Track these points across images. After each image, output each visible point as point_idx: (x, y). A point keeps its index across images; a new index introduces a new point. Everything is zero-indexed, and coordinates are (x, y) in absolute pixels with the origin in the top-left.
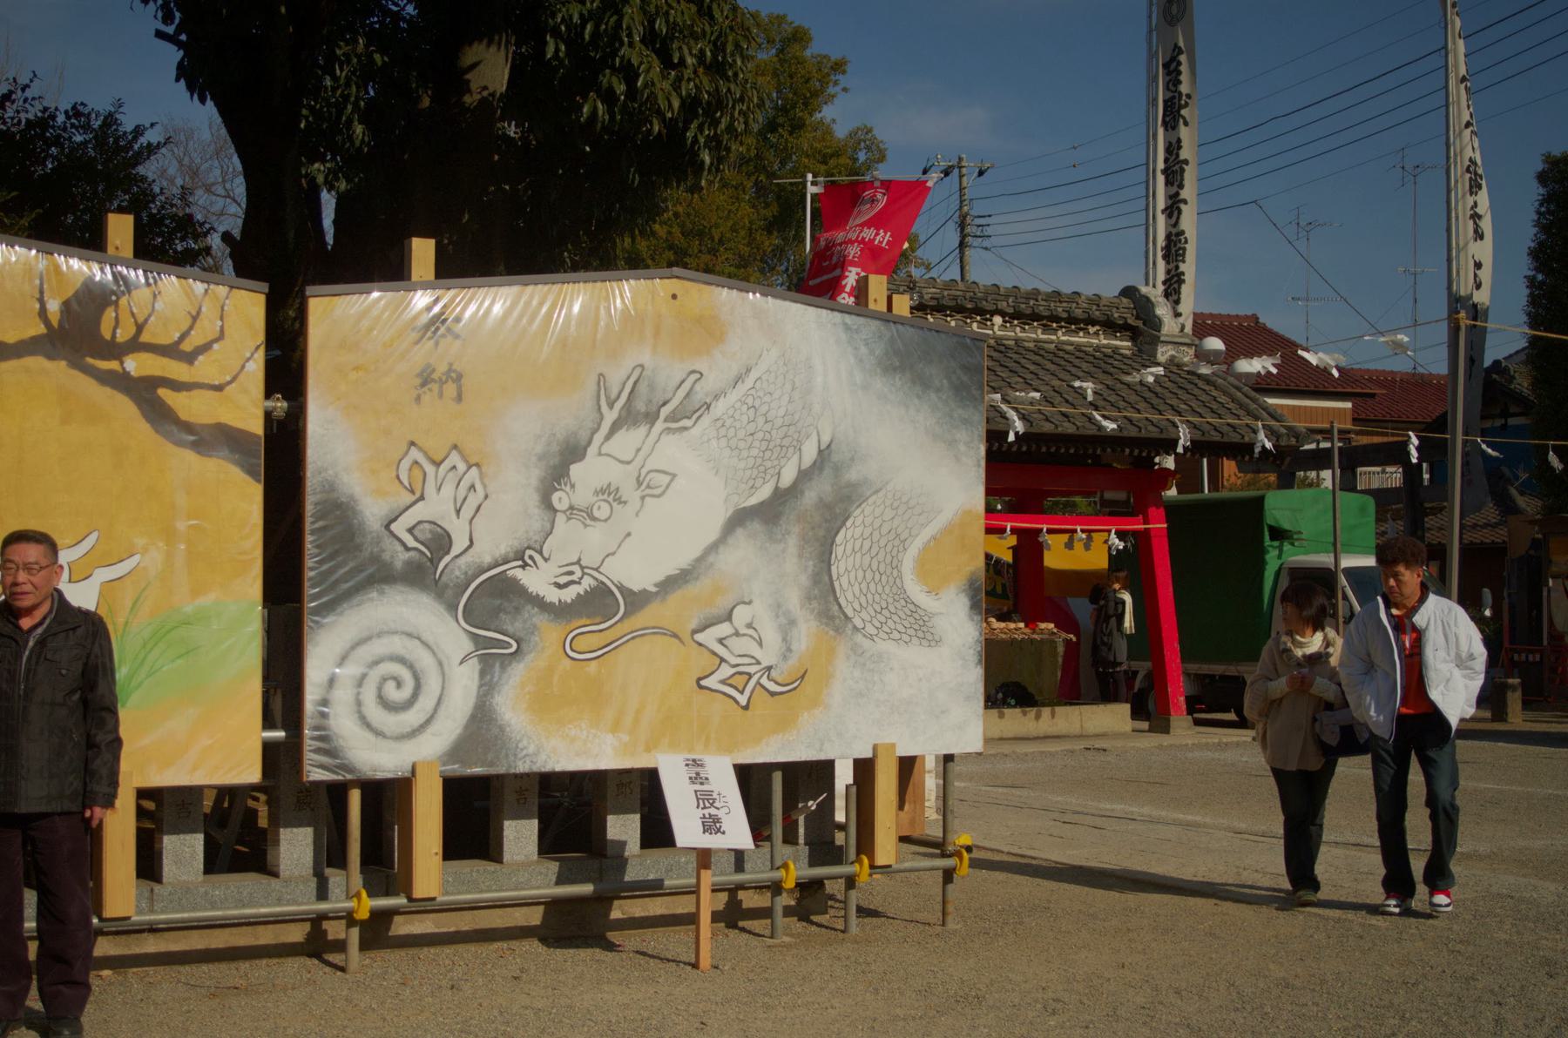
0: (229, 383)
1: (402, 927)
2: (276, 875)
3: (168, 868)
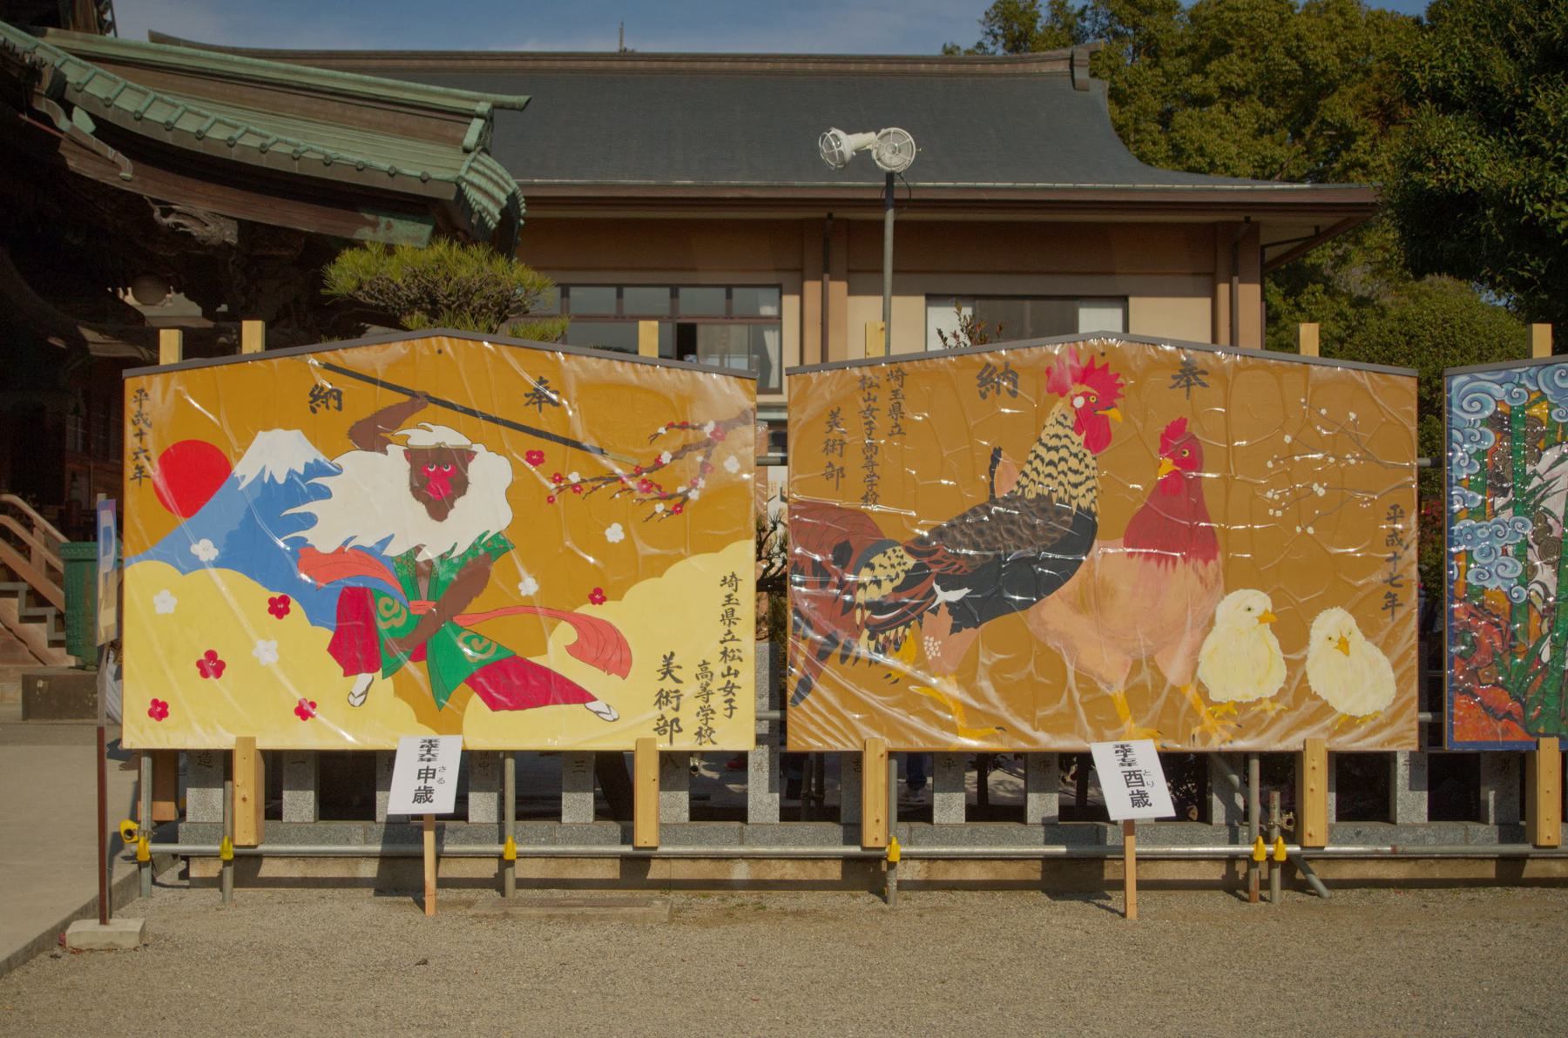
1: (1532, 869)
2: (1394, 823)
3: (289, 813)
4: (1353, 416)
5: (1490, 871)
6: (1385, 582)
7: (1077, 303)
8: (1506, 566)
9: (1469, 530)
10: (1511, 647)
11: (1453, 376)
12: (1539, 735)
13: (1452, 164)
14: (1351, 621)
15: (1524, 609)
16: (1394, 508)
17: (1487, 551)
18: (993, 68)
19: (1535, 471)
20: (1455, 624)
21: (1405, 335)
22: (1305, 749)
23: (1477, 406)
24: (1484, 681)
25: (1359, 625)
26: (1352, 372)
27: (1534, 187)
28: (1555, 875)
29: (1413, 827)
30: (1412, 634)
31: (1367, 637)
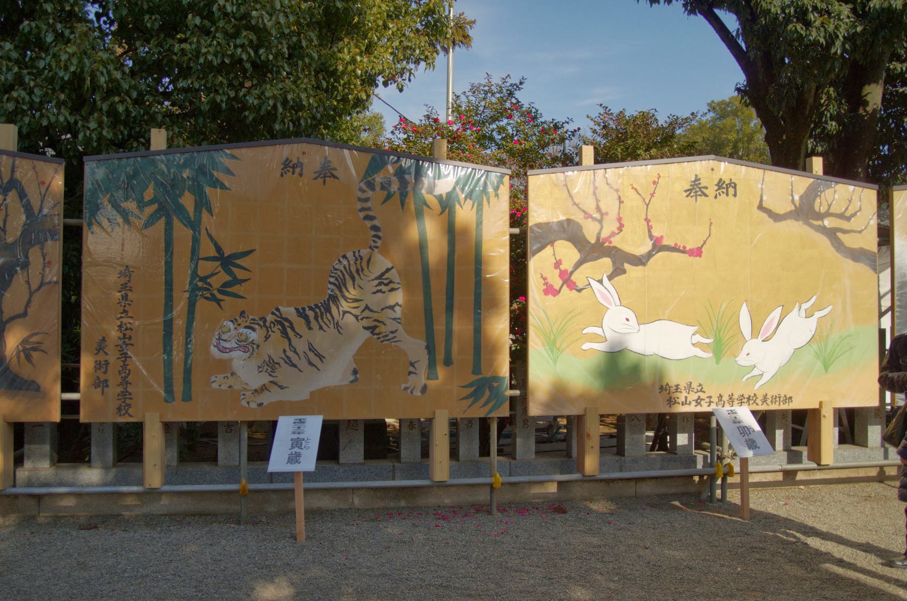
0: (864, 229)
1: (800, 476)
3: (344, 457)
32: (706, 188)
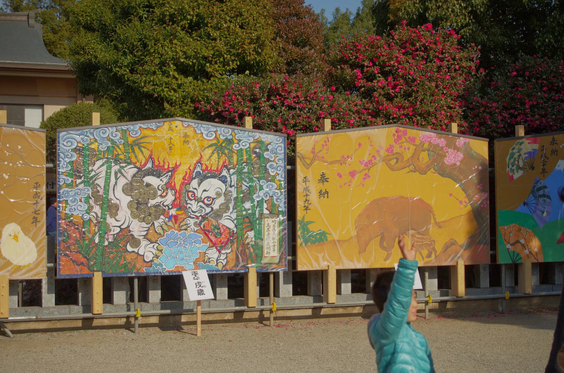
1: (246, 316)
3: (281, 294)
4: (20, 147)
5: (79, 324)
6: (32, 212)
7: (24, 107)
8: (81, 206)
9: (66, 192)
10: (83, 237)
11: (60, 132)
12: (94, 271)
13: (89, 53)
14: (18, 228)
15: (88, 223)
16: (36, 183)
17: (73, 200)
18: (8, 18)
19: (92, 169)
20: (61, 229)
21: (65, 117)
22: (328, 269)
23: (69, 144)
24: (72, 251)
25: (22, 229)
26: (19, 130)
27: (116, 62)
28: (105, 324)
29: (48, 308)
30: (44, 233)
31: (26, 235)
32: (328, 179)
